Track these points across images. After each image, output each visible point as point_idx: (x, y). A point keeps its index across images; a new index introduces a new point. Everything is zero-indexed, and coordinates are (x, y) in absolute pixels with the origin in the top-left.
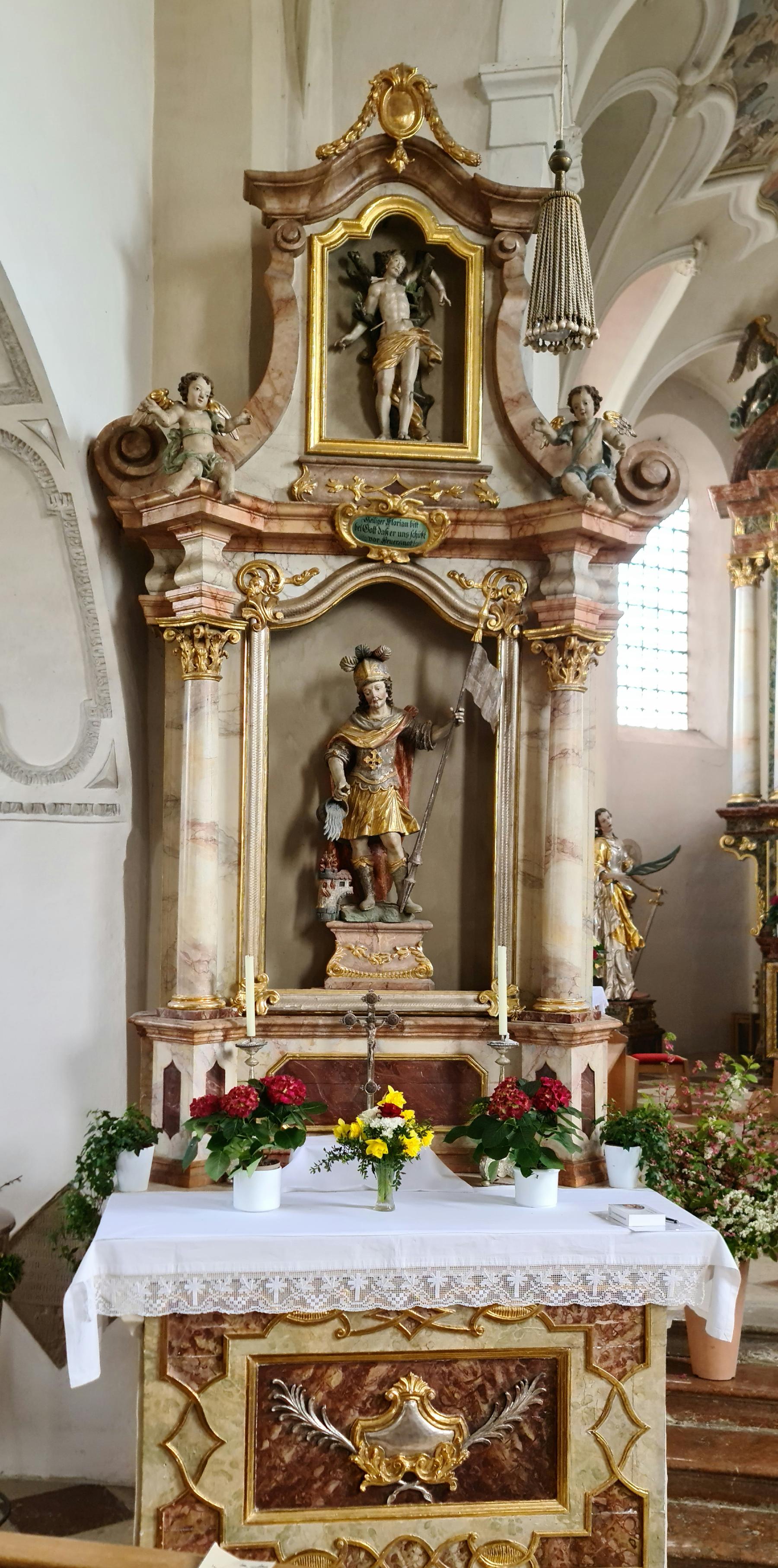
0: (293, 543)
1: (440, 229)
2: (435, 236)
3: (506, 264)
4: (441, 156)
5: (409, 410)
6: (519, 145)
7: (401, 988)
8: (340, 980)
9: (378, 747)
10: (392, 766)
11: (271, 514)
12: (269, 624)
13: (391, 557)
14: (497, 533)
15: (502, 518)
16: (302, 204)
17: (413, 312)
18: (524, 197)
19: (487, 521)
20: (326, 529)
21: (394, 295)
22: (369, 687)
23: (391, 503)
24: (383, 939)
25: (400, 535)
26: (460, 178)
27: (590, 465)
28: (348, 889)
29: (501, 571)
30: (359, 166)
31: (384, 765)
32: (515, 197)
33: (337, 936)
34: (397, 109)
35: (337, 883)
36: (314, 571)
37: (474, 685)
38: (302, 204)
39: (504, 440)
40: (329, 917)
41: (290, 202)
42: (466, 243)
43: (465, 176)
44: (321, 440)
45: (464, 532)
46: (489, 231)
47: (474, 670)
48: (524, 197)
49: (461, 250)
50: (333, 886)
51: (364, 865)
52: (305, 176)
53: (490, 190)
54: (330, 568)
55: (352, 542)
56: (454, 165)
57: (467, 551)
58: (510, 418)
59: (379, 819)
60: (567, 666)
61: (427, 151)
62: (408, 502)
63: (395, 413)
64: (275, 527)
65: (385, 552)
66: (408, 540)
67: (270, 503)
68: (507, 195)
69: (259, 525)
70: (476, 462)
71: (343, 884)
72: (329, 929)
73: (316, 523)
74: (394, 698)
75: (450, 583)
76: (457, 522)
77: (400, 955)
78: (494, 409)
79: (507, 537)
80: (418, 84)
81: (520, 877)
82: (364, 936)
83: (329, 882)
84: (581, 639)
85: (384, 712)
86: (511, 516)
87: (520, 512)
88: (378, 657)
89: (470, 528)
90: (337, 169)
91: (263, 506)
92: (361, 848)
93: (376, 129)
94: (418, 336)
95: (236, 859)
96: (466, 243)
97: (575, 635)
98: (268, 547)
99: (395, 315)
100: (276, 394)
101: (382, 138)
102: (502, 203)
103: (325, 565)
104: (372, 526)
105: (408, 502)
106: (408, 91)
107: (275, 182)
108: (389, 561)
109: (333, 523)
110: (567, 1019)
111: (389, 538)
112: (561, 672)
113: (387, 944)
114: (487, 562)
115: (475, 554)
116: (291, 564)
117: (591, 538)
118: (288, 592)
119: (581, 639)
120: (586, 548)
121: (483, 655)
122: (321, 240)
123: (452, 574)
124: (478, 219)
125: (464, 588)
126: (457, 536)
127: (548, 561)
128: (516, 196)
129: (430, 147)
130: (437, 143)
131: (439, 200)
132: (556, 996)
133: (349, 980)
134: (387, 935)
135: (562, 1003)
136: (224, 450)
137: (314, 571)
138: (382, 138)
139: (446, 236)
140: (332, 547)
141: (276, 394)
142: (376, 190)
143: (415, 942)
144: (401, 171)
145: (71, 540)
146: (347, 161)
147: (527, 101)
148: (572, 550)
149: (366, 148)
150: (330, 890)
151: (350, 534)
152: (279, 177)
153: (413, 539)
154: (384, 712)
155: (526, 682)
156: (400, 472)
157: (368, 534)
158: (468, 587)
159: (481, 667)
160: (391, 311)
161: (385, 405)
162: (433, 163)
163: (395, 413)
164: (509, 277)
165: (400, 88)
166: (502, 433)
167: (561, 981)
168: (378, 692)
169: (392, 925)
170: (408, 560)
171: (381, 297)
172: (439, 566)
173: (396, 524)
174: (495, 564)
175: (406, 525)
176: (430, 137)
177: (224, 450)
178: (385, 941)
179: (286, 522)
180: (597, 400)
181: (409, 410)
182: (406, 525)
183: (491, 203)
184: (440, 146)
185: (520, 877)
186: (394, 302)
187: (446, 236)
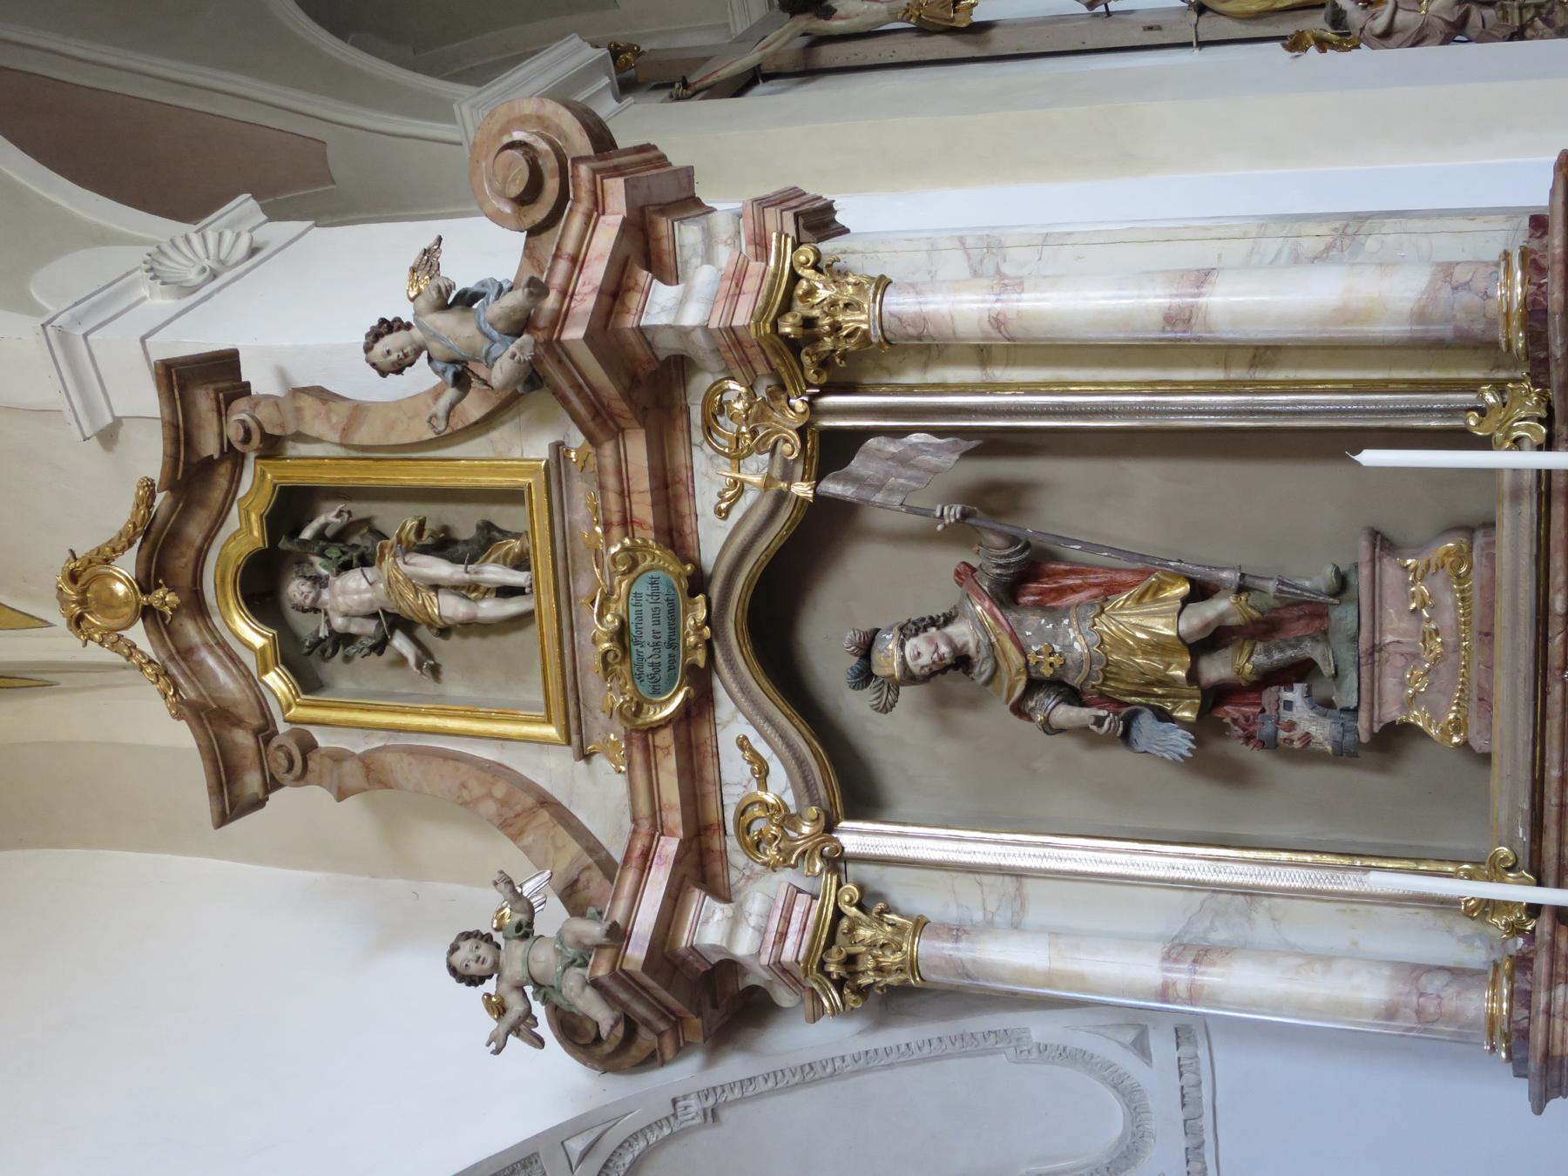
0: (702, 779)
1: (241, 532)
2: (256, 533)
3: (269, 430)
4: (152, 537)
5: (494, 573)
6: (178, 315)
7: (1490, 606)
8: (1474, 725)
9: (1023, 652)
10: (1057, 622)
11: (654, 826)
12: (830, 827)
13: (698, 629)
14: (637, 450)
15: (608, 449)
16: (243, 739)
17: (365, 561)
18: (175, 411)
19: (619, 472)
20: (665, 738)
21: (340, 599)
22: (916, 670)
23: (607, 645)
24: (1393, 632)
25: (657, 622)
26: (173, 510)
27: (479, 338)
28: (1296, 694)
29: (708, 429)
30: (185, 654)
31: (1055, 637)
32: (177, 427)
33: (1388, 720)
34: (109, 604)
35: (1286, 716)
36: (743, 743)
37: (892, 491)
38: (243, 739)
39: (512, 419)
40: (1349, 737)
41: (245, 757)
42: (255, 484)
43: (170, 500)
44: (549, 721)
45: (643, 509)
46: (233, 457)
47: (865, 494)
48: (175, 411)
49: (264, 501)
50: (1291, 726)
51: (1249, 667)
52: (205, 743)
53: (175, 468)
54: (734, 717)
55: (681, 696)
56: (160, 518)
57: (681, 489)
58: (473, 420)
59: (1158, 646)
60: (836, 328)
61: (150, 558)
62: (601, 616)
63: (506, 592)
64: (674, 818)
65: (692, 639)
66: (664, 607)
67: (634, 832)
68: (177, 441)
69: (669, 847)
70: (547, 468)
71: (1289, 705)
72: (1373, 736)
73: (660, 754)
74: (938, 611)
75: (736, 515)
76: (627, 522)
77: (1424, 604)
78: (473, 437)
79: (642, 434)
80: (73, 577)
81: (1260, 375)
82: (1388, 670)
83: (1282, 734)
84: (787, 306)
85: (962, 632)
86: (600, 436)
87: (591, 425)
88: (866, 648)
89: (635, 497)
90: (196, 688)
91: (639, 846)
92: (1216, 669)
93: (138, 634)
94: (389, 560)
95: (1241, 898)
96: (255, 484)
97: (775, 325)
98: (713, 815)
99: (368, 596)
100: (489, 795)
101: (149, 619)
102: (189, 443)
103: (733, 725)
104: (648, 670)
105: (601, 616)
106: (84, 592)
107: (221, 785)
108: (707, 630)
109: (655, 728)
110: (1534, 313)
111: (664, 638)
112: (849, 336)
113: (1404, 625)
114: (695, 450)
115: (683, 474)
116: (734, 775)
117: (615, 293)
118: (780, 787)
119: (787, 306)
120: (635, 300)
121: (836, 480)
122: (289, 707)
123: (723, 514)
124: (224, 470)
125: (742, 491)
126: (650, 521)
127: (668, 359)
128: (177, 427)
129: (144, 553)
130: (136, 546)
131: (211, 529)
132: (1492, 323)
133: (1474, 704)
134: (1387, 626)
135: (1507, 314)
136: (576, 881)
137: (743, 743)
138: (149, 619)
139: (254, 517)
140: (700, 714)
141: (489, 795)
142: (217, 620)
143: (1400, 573)
144: (177, 600)
145: (746, 1090)
146: (184, 674)
147: (95, 352)
148: (641, 330)
149: (164, 645)
150: (1297, 734)
151: (668, 701)
152: (214, 781)
153: (662, 598)
154: (962, 632)
155: (891, 373)
156: (577, 598)
157: (664, 673)
158: (730, 494)
159: (857, 481)
160: (362, 603)
161: (491, 609)
162: (162, 547)
163: (506, 592)
164: (282, 426)
165: (83, 603)
166: (503, 423)
167: (1460, 315)
168: (923, 651)
169: (1365, 620)
170: (700, 597)
171: (346, 615)
172: (713, 539)
173: (639, 629)
174: (698, 436)
175: (639, 615)
176: (132, 553)
177: (576, 881)
178: (1396, 628)
179: (664, 799)
180: (387, 327)
181: (494, 573)
182: (639, 615)
183: (194, 459)
184: (139, 540)
185: (1260, 375)
186: (348, 601)
187: (254, 517)
